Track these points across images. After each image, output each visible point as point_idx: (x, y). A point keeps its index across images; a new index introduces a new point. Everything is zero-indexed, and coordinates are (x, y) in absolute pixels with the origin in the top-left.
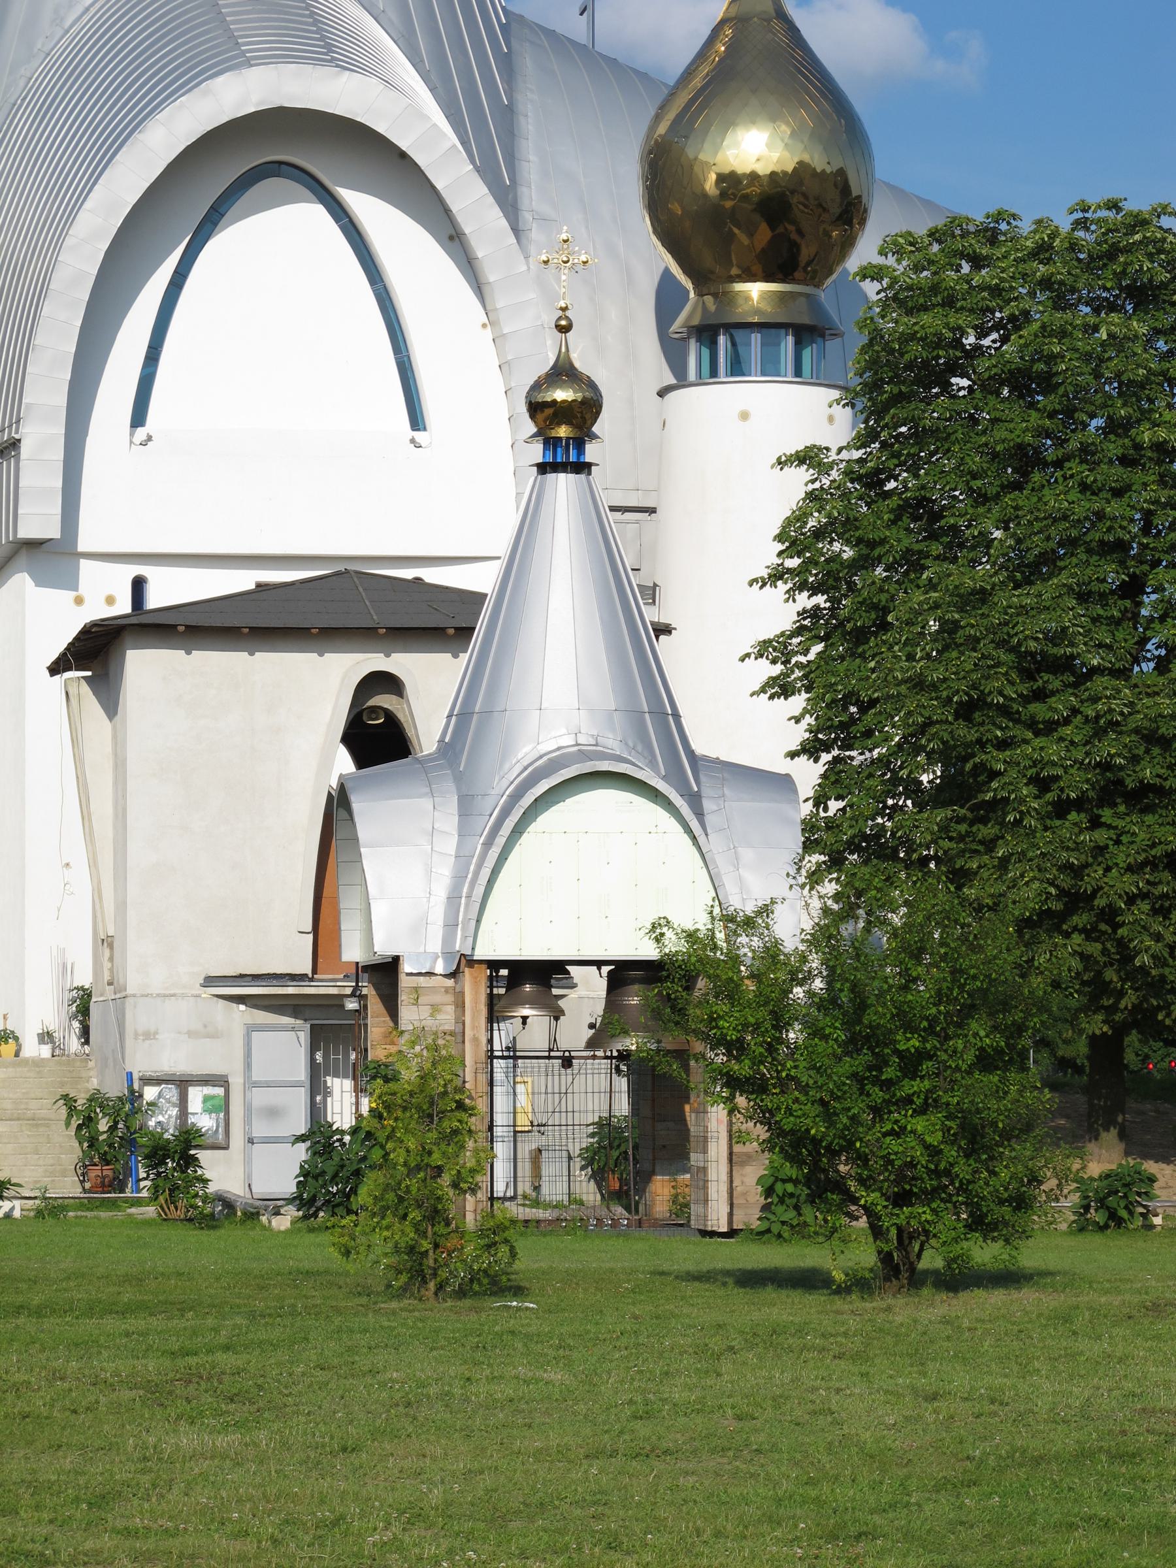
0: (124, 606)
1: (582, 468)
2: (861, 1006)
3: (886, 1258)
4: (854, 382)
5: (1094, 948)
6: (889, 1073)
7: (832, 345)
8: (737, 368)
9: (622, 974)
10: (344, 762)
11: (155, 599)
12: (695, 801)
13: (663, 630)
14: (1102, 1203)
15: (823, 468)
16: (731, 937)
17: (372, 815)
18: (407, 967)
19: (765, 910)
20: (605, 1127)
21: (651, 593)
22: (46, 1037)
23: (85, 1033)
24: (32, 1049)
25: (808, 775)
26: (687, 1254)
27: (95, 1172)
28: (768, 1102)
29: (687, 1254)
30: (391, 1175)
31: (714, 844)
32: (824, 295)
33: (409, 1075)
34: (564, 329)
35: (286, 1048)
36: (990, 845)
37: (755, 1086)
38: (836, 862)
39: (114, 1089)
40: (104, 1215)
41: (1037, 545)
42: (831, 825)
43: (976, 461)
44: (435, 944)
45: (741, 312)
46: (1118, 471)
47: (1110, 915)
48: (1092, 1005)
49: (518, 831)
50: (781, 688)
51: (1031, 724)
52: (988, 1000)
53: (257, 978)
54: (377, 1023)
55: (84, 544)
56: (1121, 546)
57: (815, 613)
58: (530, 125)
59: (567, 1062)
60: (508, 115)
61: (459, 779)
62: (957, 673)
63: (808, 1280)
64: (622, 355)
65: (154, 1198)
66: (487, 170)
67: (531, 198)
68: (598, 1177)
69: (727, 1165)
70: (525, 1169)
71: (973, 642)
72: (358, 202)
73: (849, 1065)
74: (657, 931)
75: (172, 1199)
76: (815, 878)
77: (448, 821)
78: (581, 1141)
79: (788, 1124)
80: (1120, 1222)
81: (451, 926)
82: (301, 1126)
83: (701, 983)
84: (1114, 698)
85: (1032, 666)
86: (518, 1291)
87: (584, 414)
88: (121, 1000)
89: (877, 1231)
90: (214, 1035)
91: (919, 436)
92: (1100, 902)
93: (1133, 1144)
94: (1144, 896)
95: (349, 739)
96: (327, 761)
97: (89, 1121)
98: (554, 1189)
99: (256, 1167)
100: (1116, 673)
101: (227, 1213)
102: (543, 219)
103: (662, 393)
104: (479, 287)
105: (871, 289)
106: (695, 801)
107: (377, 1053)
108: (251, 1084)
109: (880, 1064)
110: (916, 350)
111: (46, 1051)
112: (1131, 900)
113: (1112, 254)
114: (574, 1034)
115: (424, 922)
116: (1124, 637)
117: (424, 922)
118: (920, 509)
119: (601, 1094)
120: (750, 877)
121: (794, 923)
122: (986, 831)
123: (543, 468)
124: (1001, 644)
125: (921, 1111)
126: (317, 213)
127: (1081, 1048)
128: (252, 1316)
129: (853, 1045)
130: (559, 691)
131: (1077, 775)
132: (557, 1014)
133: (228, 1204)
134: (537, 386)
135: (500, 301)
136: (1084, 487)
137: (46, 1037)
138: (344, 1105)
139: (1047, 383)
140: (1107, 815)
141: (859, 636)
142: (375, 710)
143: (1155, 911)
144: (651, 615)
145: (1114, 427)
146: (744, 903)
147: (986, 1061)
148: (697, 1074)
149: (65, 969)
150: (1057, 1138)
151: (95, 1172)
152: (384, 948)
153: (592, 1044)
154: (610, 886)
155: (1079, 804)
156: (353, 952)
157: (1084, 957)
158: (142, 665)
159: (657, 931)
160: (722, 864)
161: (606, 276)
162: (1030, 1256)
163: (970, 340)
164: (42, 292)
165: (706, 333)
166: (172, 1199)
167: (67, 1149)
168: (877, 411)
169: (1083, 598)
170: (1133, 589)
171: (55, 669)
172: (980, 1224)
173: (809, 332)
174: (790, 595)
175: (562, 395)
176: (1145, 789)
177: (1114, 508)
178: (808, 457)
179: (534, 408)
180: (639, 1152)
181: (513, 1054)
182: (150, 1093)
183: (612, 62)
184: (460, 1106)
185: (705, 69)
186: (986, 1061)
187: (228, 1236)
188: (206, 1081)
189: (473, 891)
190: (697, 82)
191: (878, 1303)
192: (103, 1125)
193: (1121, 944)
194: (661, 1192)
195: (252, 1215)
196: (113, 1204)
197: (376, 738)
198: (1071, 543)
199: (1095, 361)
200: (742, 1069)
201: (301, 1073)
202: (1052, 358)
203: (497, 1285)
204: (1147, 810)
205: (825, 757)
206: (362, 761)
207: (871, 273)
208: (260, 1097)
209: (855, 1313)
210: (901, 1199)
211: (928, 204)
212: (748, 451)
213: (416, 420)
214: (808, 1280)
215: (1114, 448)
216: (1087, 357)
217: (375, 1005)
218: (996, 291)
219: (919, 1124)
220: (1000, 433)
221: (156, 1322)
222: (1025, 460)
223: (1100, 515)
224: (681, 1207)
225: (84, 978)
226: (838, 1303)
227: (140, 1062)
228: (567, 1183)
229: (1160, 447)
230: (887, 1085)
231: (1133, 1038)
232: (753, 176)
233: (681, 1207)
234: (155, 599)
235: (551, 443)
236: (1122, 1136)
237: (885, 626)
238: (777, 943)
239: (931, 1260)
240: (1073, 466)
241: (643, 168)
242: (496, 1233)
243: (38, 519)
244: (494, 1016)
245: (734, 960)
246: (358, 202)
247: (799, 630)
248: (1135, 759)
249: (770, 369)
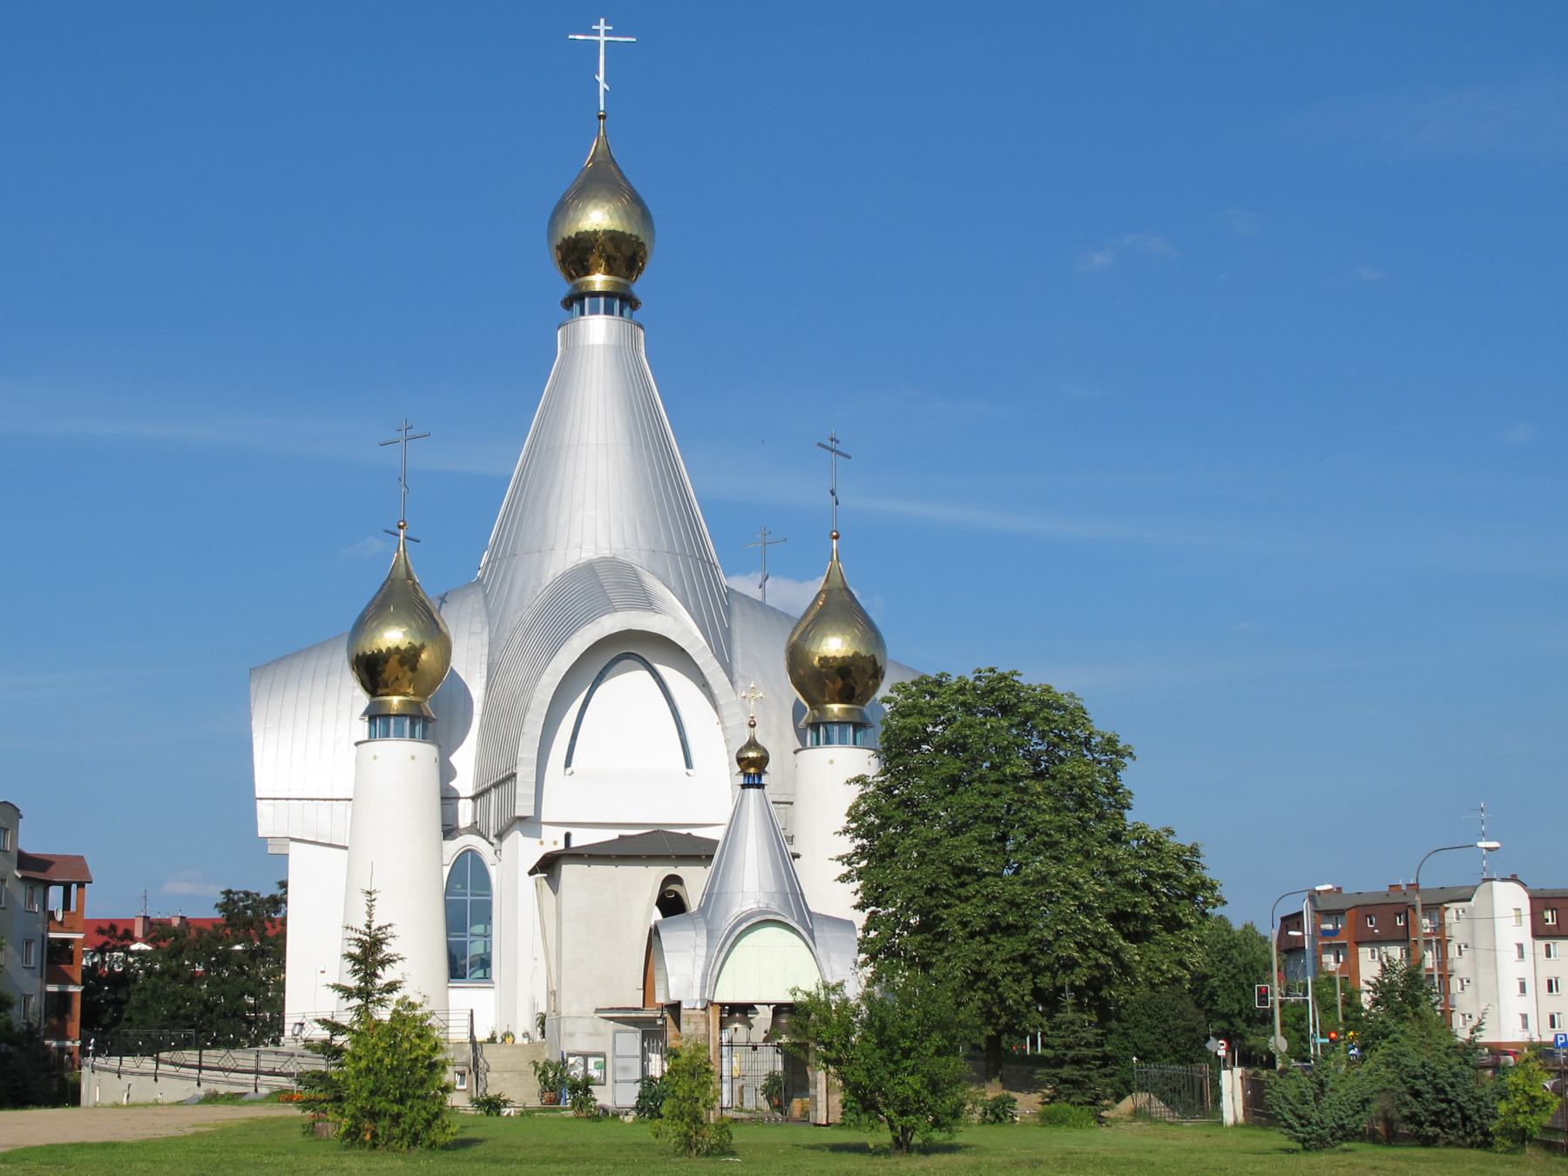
0: (561, 846)
1: (760, 786)
2: (883, 1027)
3: (896, 1139)
4: (880, 747)
5: (988, 997)
6: (896, 1057)
7: (870, 731)
8: (828, 741)
9: (779, 1009)
10: (657, 915)
11: (574, 843)
12: (811, 933)
13: (796, 856)
14: (992, 1111)
15: (866, 784)
16: (827, 996)
17: (668, 939)
18: (684, 1006)
19: (841, 984)
20: (772, 1077)
21: (791, 839)
22: (526, 1035)
23: (543, 1033)
24: (520, 1040)
25: (860, 918)
26: (807, 1135)
27: (547, 1095)
28: (844, 1069)
29: (807, 1135)
30: (676, 1097)
31: (819, 951)
32: (866, 709)
33: (685, 1054)
34: (753, 726)
35: (631, 1040)
36: (941, 951)
37: (838, 1062)
38: (873, 958)
39: (555, 1059)
40: (551, 1115)
41: (960, 819)
42: (872, 941)
43: (932, 782)
44: (697, 997)
45: (830, 717)
46: (995, 786)
47: (995, 982)
48: (988, 1022)
49: (733, 945)
50: (844, 878)
51: (959, 898)
52: (943, 1026)
53: (611, 1009)
54: (671, 1030)
55: (543, 819)
56: (997, 820)
57: (863, 847)
58: (737, 636)
59: (755, 1048)
60: (728, 632)
61: (707, 923)
62: (926, 875)
63: (861, 1149)
64: (778, 737)
65: (573, 1108)
66: (719, 656)
67: (739, 668)
68: (769, 1098)
69: (825, 1096)
70: (736, 1096)
71: (933, 862)
72: (663, 670)
73: (879, 1053)
74: (794, 992)
75: (581, 1108)
76: (864, 964)
77: (702, 940)
78: (763, 1082)
79: (852, 1079)
80: (1001, 1120)
81: (703, 987)
82: (639, 1077)
83: (813, 1017)
84: (994, 886)
85: (958, 872)
86: (733, 1154)
87: (761, 763)
88: (559, 1019)
89: (892, 1128)
90: (599, 1035)
91: (909, 771)
92: (990, 976)
93: (1006, 1084)
94: (1009, 973)
95: (658, 904)
96: (649, 914)
97: (544, 1072)
98: (749, 1104)
99: (618, 1094)
100: (995, 875)
101: (605, 1115)
102: (743, 677)
103: (795, 752)
104: (716, 707)
105: (887, 707)
106: (811, 933)
107: (672, 1043)
108: (615, 1056)
109: (893, 1053)
110: (906, 734)
111: (526, 1041)
112: (1004, 975)
113: (992, 691)
114: (758, 1035)
115: (691, 986)
116: (1000, 860)
117: (691, 986)
118: (908, 803)
119: (771, 1062)
120: (836, 968)
121: (854, 990)
122: (940, 945)
123: (744, 786)
124: (945, 862)
125: (911, 1074)
126: (646, 674)
127: (983, 1043)
128: (615, 1164)
129: (880, 1045)
130: (751, 883)
131: (979, 920)
132: (750, 1027)
133: (605, 1111)
134: (741, 751)
135: (725, 713)
136: (981, 793)
137: (526, 1035)
138: (657, 1066)
139: (964, 748)
140: (992, 938)
141: (882, 858)
142: (671, 892)
143: (1014, 981)
144: (791, 849)
145: (993, 767)
146: (833, 982)
147: (939, 1052)
148: (812, 1059)
149: (534, 1005)
150: (972, 1080)
151: (547, 1095)
152: (674, 997)
153: (765, 1040)
154: (774, 970)
155: (980, 933)
156: (660, 999)
157: (984, 1002)
158: (568, 871)
159: (794, 992)
160: (823, 960)
161: (771, 701)
162: (959, 1139)
163: (930, 729)
164: (526, 709)
165: (814, 726)
166: (581, 1108)
167: (534, 1085)
168: (890, 760)
169: (981, 842)
170: (1003, 838)
171: (531, 873)
172: (937, 1124)
173: (860, 726)
174: (852, 840)
175: (752, 755)
176: (1009, 926)
177: (994, 802)
178: (860, 780)
179: (740, 760)
180: (787, 1087)
181: (731, 1044)
182: (571, 1060)
183: (773, 609)
184: (707, 1070)
185: (813, 612)
186: (939, 1052)
187: (606, 1124)
188: (596, 1055)
189: (712, 975)
190: (810, 618)
191: (893, 1160)
192: (550, 1074)
193: (1000, 995)
194: (796, 1104)
195: (616, 1116)
196: (554, 1110)
197: (671, 904)
198: (976, 818)
199: (985, 738)
200: (833, 1055)
201: (638, 1052)
202: (966, 737)
203: (723, 1150)
204: (1010, 935)
205: (868, 911)
206: (665, 914)
207: (887, 700)
208: (620, 1062)
209: (882, 1164)
210: (903, 1113)
211: (912, 670)
212: (833, 779)
213: (689, 764)
214: (861, 1149)
215: (993, 776)
216: (981, 736)
217: (670, 1022)
218: (942, 707)
219: (911, 1080)
220: (943, 770)
221: (573, 1167)
222: (955, 781)
223: (987, 806)
224: (805, 1113)
225: (543, 1009)
226: (876, 1160)
227: (567, 1047)
228: (756, 1101)
229: (1014, 775)
230: (895, 1063)
231: (1005, 1037)
232: (835, 658)
233: (805, 1113)
234: (574, 843)
235: (747, 775)
236: (1001, 1080)
237: (892, 854)
238: (847, 1000)
239: (916, 1140)
240: (976, 785)
241: (571, 214)
242: (723, 1127)
243: (524, 808)
244: (722, 1027)
245: (827, 1004)
246: (663, 670)
247: (856, 854)
248: (1005, 913)
249: (843, 741)
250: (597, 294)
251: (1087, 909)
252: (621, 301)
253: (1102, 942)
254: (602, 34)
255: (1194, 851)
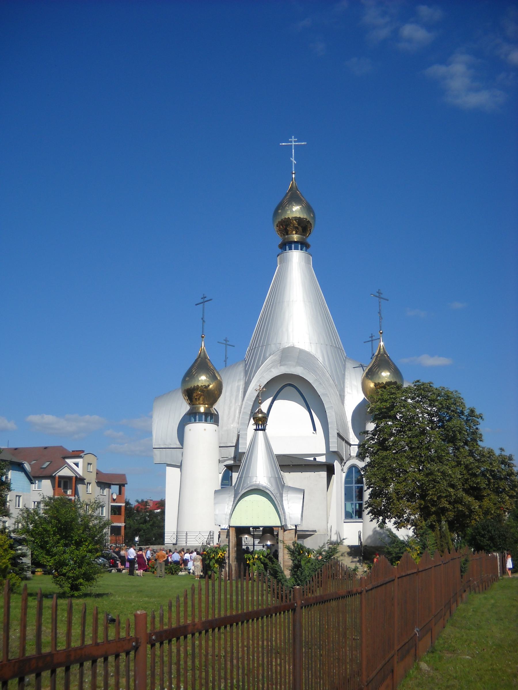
1: (212, 417)
64: (503, 453)
123: (256, 430)
250: (295, 242)
251: (453, 486)
252: (303, 245)
253: (459, 501)
254: (293, 142)
255: (510, 458)
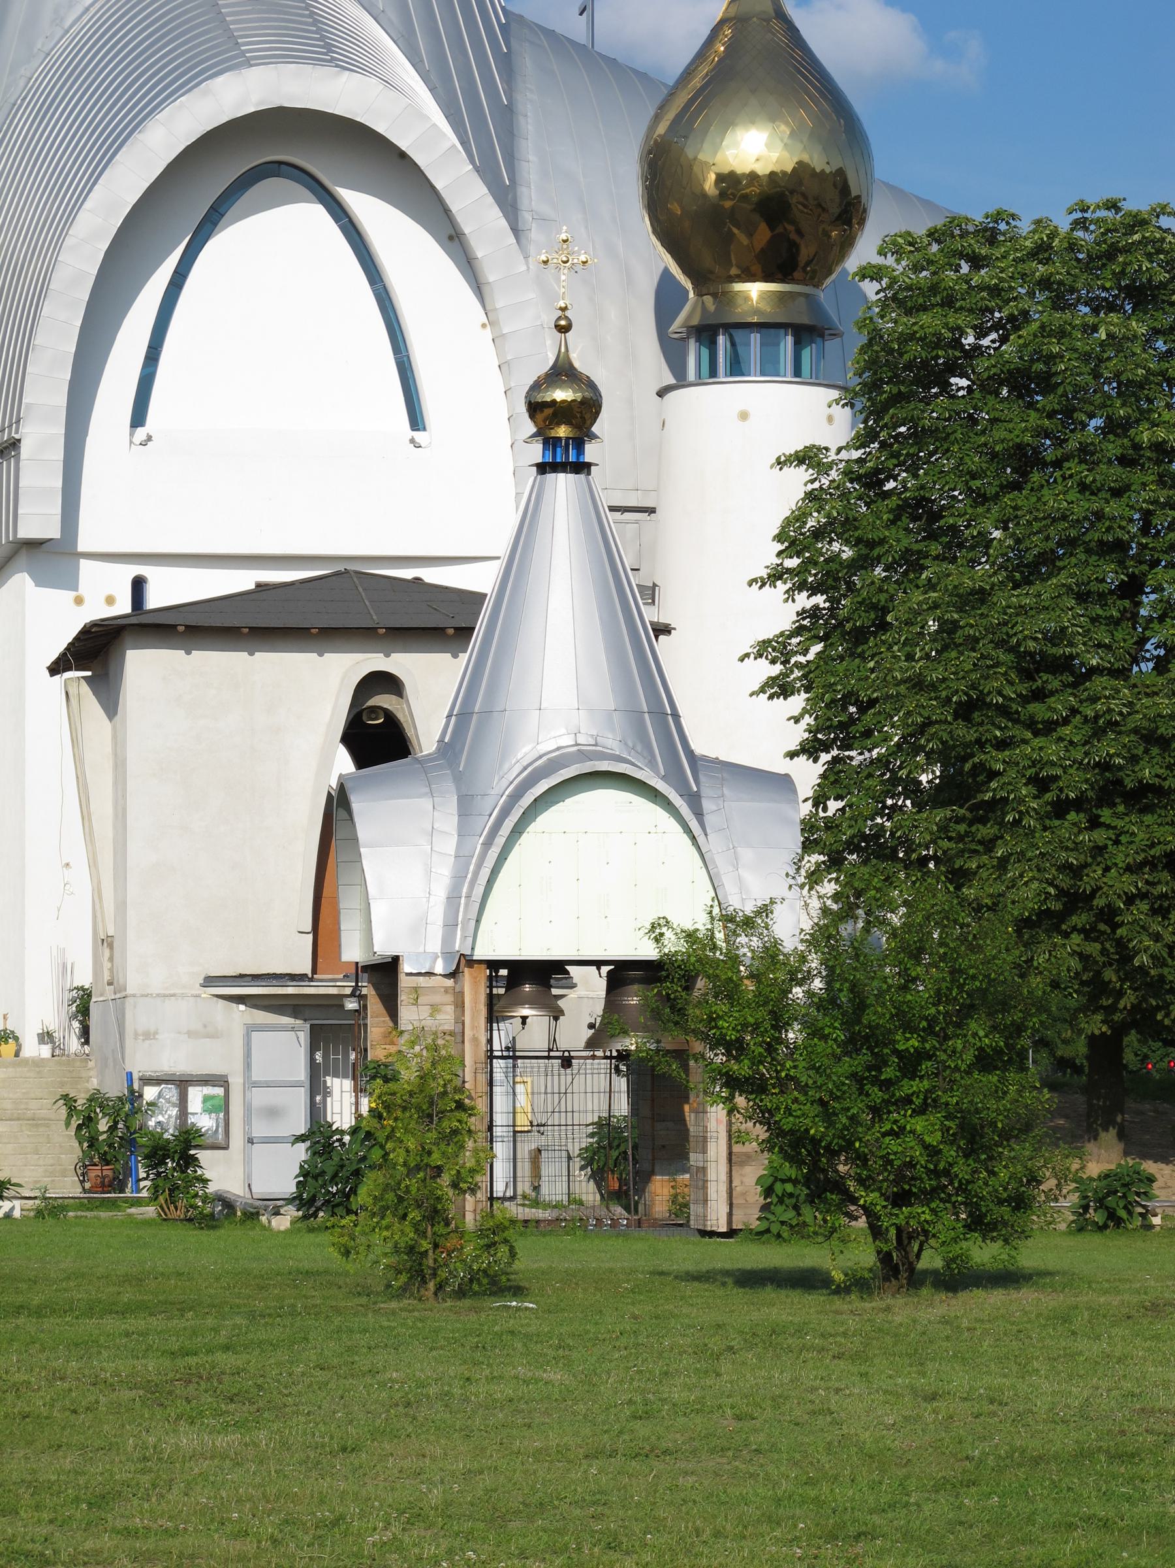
0: (124, 606)
1: (581, 468)
2: (860, 1006)
3: (885, 1258)
4: (854, 382)
5: (1093, 948)
6: (888, 1073)
7: (831, 345)
8: (737, 368)
9: (622, 974)
10: (344, 762)
11: (155, 599)
12: (694, 801)
13: (662, 630)
14: (1101, 1203)
15: (822, 468)
16: (730, 937)
17: (372, 815)
18: (406, 967)
19: (765, 910)
20: (605, 1127)
21: (650, 593)
22: (46, 1037)
23: (85, 1033)
24: (32, 1049)
25: (807, 775)
26: (686, 1254)
27: (94, 1172)
28: (768, 1102)
29: (686, 1254)
30: (391, 1175)
31: (714, 844)
32: (823, 295)
33: (408, 1075)
34: (564, 329)
35: (286, 1048)
36: (989, 845)
37: (754, 1086)
38: (835, 862)
39: (114, 1089)
40: (104, 1215)
41: (1036, 545)
42: (831, 825)
43: (975, 461)
44: (434, 944)
45: (741, 312)
46: (1117, 471)
47: (1109, 915)
48: (1092, 1005)
49: (518, 831)
51: (1031, 724)
52: (987, 1000)
54: (376, 1023)
55: (84, 544)
56: (1120, 546)
57: (814, 613)
58: (529, 125)
59: (567, 1062)
60: (507, 115)
61: (458, 779)
62: (956, 673)
63: (808, 1280)
64: (621, 355)
65: (154, 1198)
66: (487, 170)
67: (531, 198)
68: (598, 1177)
69: (726, 1165)
70: (525, 1169)
71: (972, 642)
72: (358, 202)
73: (848, 1065)
74: (656, 931)
75: (172, 1199)
76: (814, 878)
77: (448, 821)
79: (788, 1124)
80: (1119, 1222)
81: (450, 926)
82: (301, 1126)
83: (701, 983)
84: (1113, 698)
85: (1032, 666)
86: (518, 1291)
87: (583, 414)
88: (121, 1000)
89: (876, 1231)
90: (214, 1035)
91: (919, 436)
92: (1099, 902)
93: (1132, 1144)
94: (1143, 896)
95: (348, 739)
96: (326, 761)
97: (89, 1121)
98: (554, 1189)
99: (256, 1167)
100: (1115, 673)
101: (227, 1213)
102: (543, 219)
103: (661, 393)
104: (478, 287)
105: (870, 289)
106: (694, 801)
107: (377, 1053)
108: (251, 1084)
109: (879, 1064)
110: (915, 350)
111: (45, 1051)
112: (1130, 900)
113: (1111, 254)
114: (574, 1034)
115: (423, 922)
116: (1123, 637)
117: (423, 922)
118: (919, 509)
119: (601, 1094)
120: (749, 877)
121: (793, 923)
122: (986, 831)
123: (543, 468)
124: (1000, 644)
125: (921, 1111)
126: (316, 213)
127: (1081, 1048)
128: (252, 1316)
129: (852, 1045)
130: (558, 691)
131: (1076, 775)
132: (557, 1014)
133: (228, 1204)
134: (536, 386)
135: (500, 301)
136: (1083, 487)
137: (46, 1037)
138: (344, 1105)
139: (1046, 383)
140: (1106, 815)
141: (859, 636)
142: (375, 710)
143: (1154, 911)
144: (651, 615)
145: (1113, 427)
146: (743, 903)
147: (985, 1061)
148: (697, 1074)
149: (65, 969)
150: (1056, 1138)
151: (94, 1172)
152: (383, 948)
153: (591, 1044)
154: (610, 886)
155: (1078, 804)
156: (352, 952)
157: (1083, 957)
158: (142, 665)
159: (656, 931)
160: (721, 864)
161: (606, 276)
162: (1029, 1256)
163: (969, 340)
164: (42, 292)
165: (706, 333)
166: (172, 1199)
167: (66, 1149)
168: (877, 411)
169: (1082, 598)
170: (1132, 589)
171: (55, 669)
172: (980, 1224)
173: (808, 332)
174: (790, 595)
175: (561, 395)
176: (1144, 789)
177: (1113, 508)
178: (807, 457)
179: (534, 408)
180: (638, 1152)
181: (512, 1054)
182: (150, 1093)
183: (612, 62)
184: (460, 1106)
185: (704, 69)
186: (985, 1061)
187: (228, 1236)
188: (205, 1081)
189: (473, 891)
190: (697, 82)
191: (877, 1303)
192: (103, 1125)
193: (1121, 944)
194: (660, 1192)
195: (252, 1215)
196: (113, 1204)
197: (375, 738)
198: (1070, 543)
199: (1094, 361)
200: (741, 1069)
201: (301, 1073)
202: (1051, 358)
203: (497, 1285)
204: (1146, 810)
205: (825, 757)
206: (362, 761)
207: (870, 273)
208: (260, 1097)
209: (854, 1313)
210: (900, 1199)
211: (928, 204)
212: (747, 451)
213: (416, 420)
214: (808, 1280)
215: (1113, 448)
216: (1086, 357)
217: (375, 1005)
218: (995, 291)
219: (918, 1124)
220: (999, 433)
221: (155, 1322)
222: (1024, 460)
223: (1099, 515)
224: (680, 1207)
225: (84, 978)
226: (838, 1303)
227: (140, 1062)
228: (566, 1183)
229: (1159, 447)
230: (887, 1085)
231: (1132, 1038)
232: (753, 176)
233: (680, 1207)
234: (155, 599)
235: (550, 443)
236: (1121, 1136)
237: (884, 626)
238: (776, 943)
239: (930, 1260)
240: (1073, 466)
242: (495, 1233)
243: (38, 519)
244: (493, 1016)
245: (734, 960)
246: (358, 202)
247: (799, 630)
248: (1134, 759)
249: (769, 369)
